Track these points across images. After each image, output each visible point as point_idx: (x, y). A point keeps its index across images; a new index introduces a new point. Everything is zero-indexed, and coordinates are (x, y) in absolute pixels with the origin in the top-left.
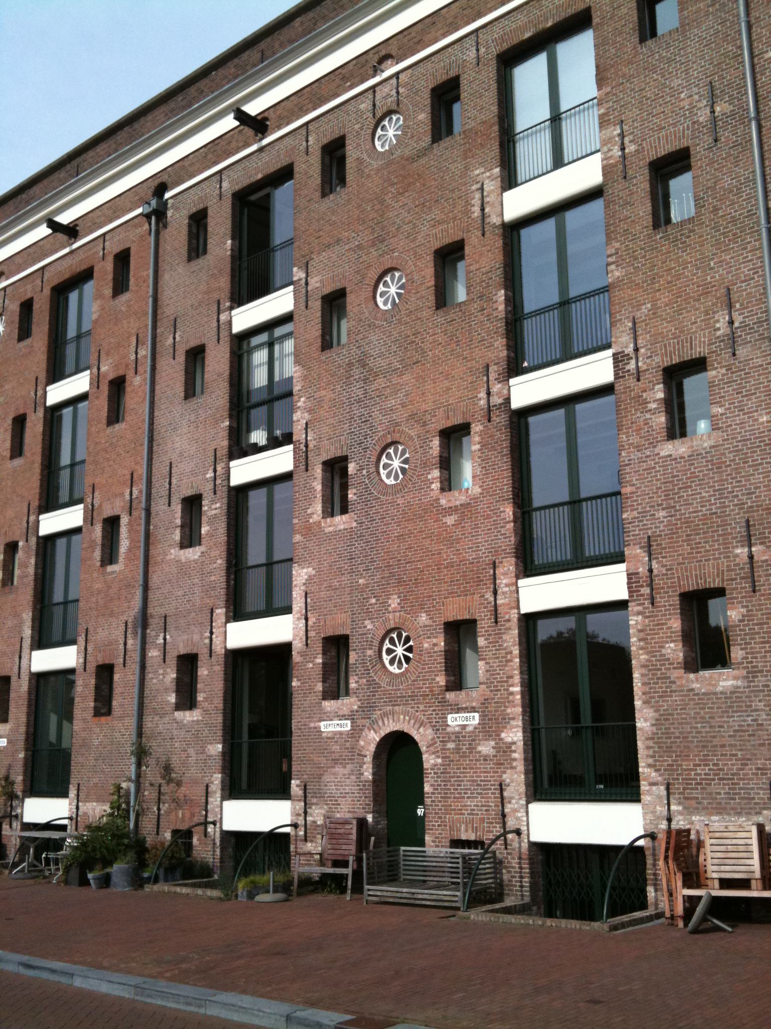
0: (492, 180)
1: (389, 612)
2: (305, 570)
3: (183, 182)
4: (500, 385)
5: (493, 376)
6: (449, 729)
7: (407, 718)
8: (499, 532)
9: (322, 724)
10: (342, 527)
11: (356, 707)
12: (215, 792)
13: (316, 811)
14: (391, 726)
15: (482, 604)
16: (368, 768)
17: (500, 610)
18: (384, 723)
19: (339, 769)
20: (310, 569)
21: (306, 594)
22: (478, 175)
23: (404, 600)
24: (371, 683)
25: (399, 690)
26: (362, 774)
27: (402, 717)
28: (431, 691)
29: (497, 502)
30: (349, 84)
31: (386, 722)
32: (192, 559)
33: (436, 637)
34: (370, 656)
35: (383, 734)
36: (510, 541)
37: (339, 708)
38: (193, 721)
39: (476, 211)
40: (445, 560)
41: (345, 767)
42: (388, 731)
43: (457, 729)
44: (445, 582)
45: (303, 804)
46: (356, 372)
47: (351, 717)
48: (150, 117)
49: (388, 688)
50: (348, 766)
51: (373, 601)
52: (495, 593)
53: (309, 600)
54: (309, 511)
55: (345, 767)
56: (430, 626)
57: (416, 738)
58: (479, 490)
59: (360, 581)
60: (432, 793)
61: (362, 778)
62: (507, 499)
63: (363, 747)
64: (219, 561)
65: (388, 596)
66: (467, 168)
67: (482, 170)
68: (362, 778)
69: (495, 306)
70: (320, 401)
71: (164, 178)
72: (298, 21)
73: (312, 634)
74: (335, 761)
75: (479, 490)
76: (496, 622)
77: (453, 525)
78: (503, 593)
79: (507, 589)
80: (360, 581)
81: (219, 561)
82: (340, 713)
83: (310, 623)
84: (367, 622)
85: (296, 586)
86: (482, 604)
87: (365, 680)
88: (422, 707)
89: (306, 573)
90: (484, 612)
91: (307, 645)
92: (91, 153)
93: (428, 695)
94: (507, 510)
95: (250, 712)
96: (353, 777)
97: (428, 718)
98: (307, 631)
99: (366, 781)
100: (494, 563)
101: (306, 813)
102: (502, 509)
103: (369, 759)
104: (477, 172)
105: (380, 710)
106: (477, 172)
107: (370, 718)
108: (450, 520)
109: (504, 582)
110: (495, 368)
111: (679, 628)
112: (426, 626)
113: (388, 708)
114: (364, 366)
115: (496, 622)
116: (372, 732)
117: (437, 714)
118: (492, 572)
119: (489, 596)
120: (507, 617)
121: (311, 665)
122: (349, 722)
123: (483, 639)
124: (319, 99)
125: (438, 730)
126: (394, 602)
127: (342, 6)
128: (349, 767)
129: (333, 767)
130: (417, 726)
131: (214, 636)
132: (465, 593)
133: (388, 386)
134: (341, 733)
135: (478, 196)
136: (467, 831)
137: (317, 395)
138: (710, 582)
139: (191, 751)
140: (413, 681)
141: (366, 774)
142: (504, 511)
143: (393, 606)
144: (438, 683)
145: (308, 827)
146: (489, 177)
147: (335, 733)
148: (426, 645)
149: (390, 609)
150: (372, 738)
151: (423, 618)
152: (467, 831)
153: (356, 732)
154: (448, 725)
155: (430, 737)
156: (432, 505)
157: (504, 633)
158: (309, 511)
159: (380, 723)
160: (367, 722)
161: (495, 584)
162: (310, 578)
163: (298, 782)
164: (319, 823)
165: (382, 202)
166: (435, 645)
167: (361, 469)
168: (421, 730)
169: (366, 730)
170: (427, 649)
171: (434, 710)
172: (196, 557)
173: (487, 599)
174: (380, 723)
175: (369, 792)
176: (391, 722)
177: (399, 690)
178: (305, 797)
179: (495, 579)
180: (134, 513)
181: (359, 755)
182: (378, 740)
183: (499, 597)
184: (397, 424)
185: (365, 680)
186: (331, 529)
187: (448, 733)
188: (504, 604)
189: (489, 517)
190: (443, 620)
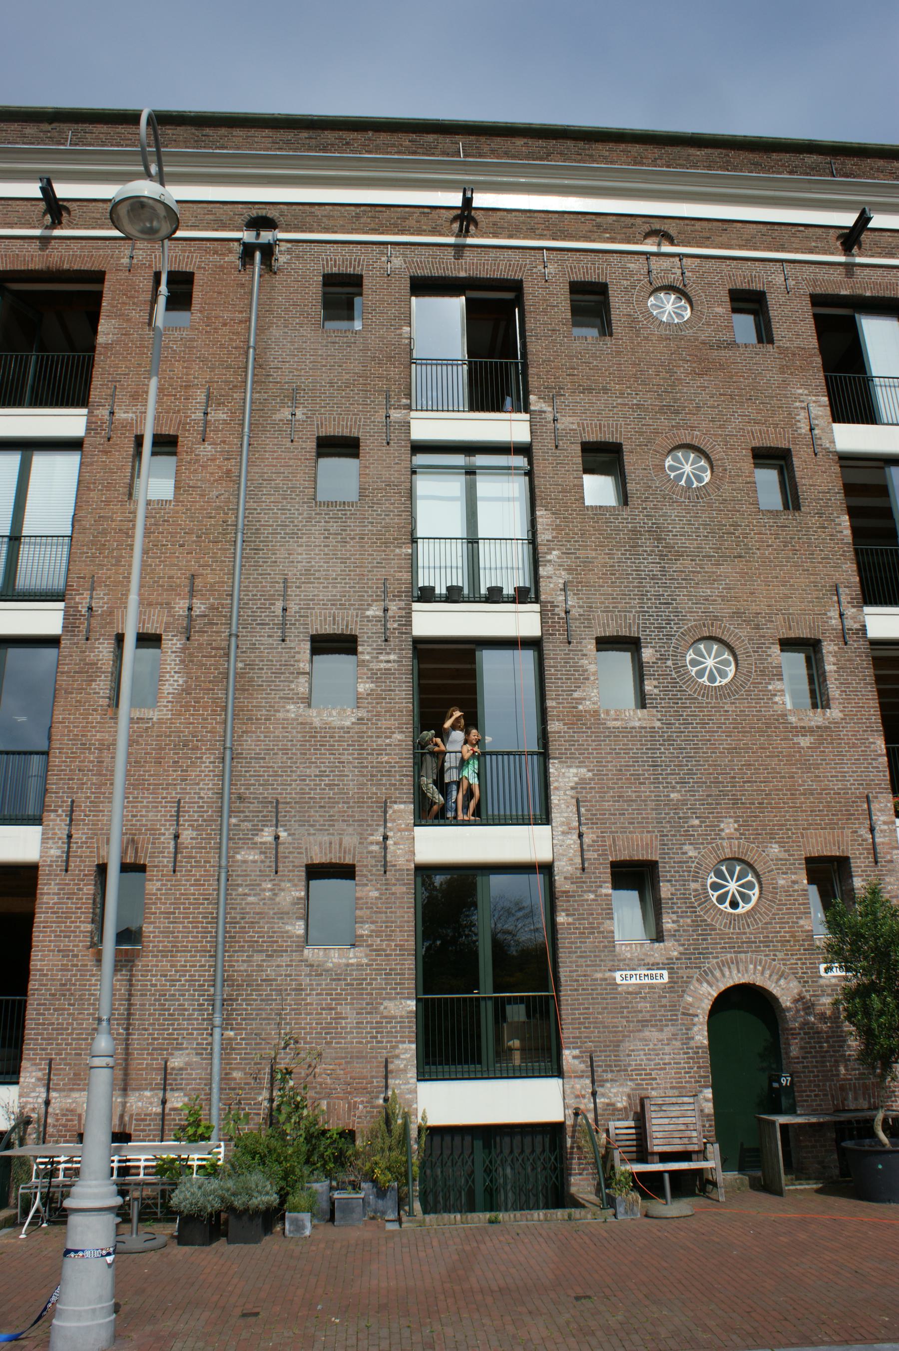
0: (820, 406)
1: (723, 839)
2: (573, 770)
3: (311, 231)
4: (854, 610)
5: (844, 599)
6: (822, 981)
7: (759, 968)
8: (870, 764)
9: (618, 975)
10: (637, 724)
11: (675, 953)
12: (405, 1071)
13: (614, 1090)
14: (734, 978)
15: (855, 840)
16: (700, 1030)
17: (879, 848)
18: (723, 975)
19: (652, 1034)
20: (583, 770)
21: (578, 801)
22: (797, 408)
23: (743, 826)
24: (698, 923)
25: (745, 933)
26: (693, 1038)
27: (752, 966)
28: (793, 936)
29: (864, 731)
30: (608, 235)
31: (727, 973)
32: (337, 723)
33: (795, 873)
34: (696, 890)
35: (722, 987)
36: (884, 776)
37: (646, 955)
38: (348, 965)
39: (804, 429)
40: (800, 785)
41: (662, 1030)
42: (730, 983)
43: (834, 981)
44: (802, 811)
45: (588, 1081)
46: (646, 543)
47: (669, 965)
48: (238, 132)
49: (727, 930)
50: (665, 1029)
51: (696, 822)
52: (872, 830)
53: (583, 810)
54: (576, 695)
55: (662, 1030)
56: (786, 860)
57: (775, 992)
58: (841, 715)
59: (672, 795)
60: (803, 1058)
61: (692, 1044)
62: (877, 731)
63: (691, 1005)
64: (398, 736)
65: (720, 818)
66: (785, 384)
67: (806, 392)
68: (692, 1044)
69: (838, 528)
70: (587, 563)
71: (272, 213)
72: (550, 703)
73: (590, 855)
74: (644, 1023)
75: (841, 715)
76: (876, 862)
77: (808, 748)
78: (881, 831)
79: (886, 827)
80: (672, 795)
81: (398, 736)
82: (651, 960)
83: (587, 840)
84: (686, 848)
85: (556, 788)
86: (855, 840)
87: (689, 920)
88: (780, 955)
89: (576, 775)
90: (858, 849)
91: (583, 869)
92: (104, 128)
93: (789, 941)
94: (879, 742)
95: (475, 955)
96: (678, 1044)
97: (791, 969)
98: (582, 850)
99: (697, 1047)
100: (867, 797)
101: (594, 1094)
102: (871, 740)
103: (702, 1019)
104: (800, 391)
105: (717, 957)
106: (800, 391)
107: (700, 968)
108: (805, 742)
109: (882, 818)
110: (847, 590)
111: (855, 879)
112: (781, 860)
113: (729, 956)
114: (659, 539)
115: (876, 862)
116: (705, 985)
117: (803, 964)
118: (866, 806)
119: (864, 832)
120: (889, 857)
121: (592, 896)
122: (665, 973)
123: (860, 879)
124: (562, 232)
125: (807, 982)
126: (729, 827)
127: (591, 156)
128: (669, 1031)
129: (640, 1031)
130: (775, 977)
131: (390, 842)
132: (832, 826)
133: (699, 572)
134: (652, 986)
135: (803, 414)
136: (856, 1099)
137: (581, 553)
138: (665, 867)
139: (346, 1010)
140: (766, 923)
141: (697, 1038)
142: (874, 743)
143: (727, 831)
144: (802, 926)
145: (599, 1111)
146: (814, 402)
147: (642, 986)
148: (781, 882)
149: (723, 834)
150: (706, 993)
151: (775, 849)
152: (856, 1099)
153: (677, 985)
154: (821, 977)
155: (796, 991)
156: (777, 720)
157: (886, 875)
158: (576, 695)
159: (717, 973)
160: (696, 974)
161: (871, 819)
162: (582, 782)
163: (576, 1052)
164: (619, 1105)
165: (671, 372)
166: (794, 882)
167: (663, 658)
168: (782, 982)
169: (694, 981)
170: (783, 887)
171: (800, 959)
172: (348, 723)
173: (861, 836)
174: (717, 973)
175: (705, 1060)
176: (735, 972)
177: (745, 933)
178: (593, 1071)
179: (870, 814)
180: (195, 637)
181: (684, 1014)
182: (715, 995)
183: (877, 835)
184: (716, 618)
185: (689, 920)
186: (618, 724)
187: (821, 986)
188: (883, 843)
189: (854, 746)
190: (804, 854)
